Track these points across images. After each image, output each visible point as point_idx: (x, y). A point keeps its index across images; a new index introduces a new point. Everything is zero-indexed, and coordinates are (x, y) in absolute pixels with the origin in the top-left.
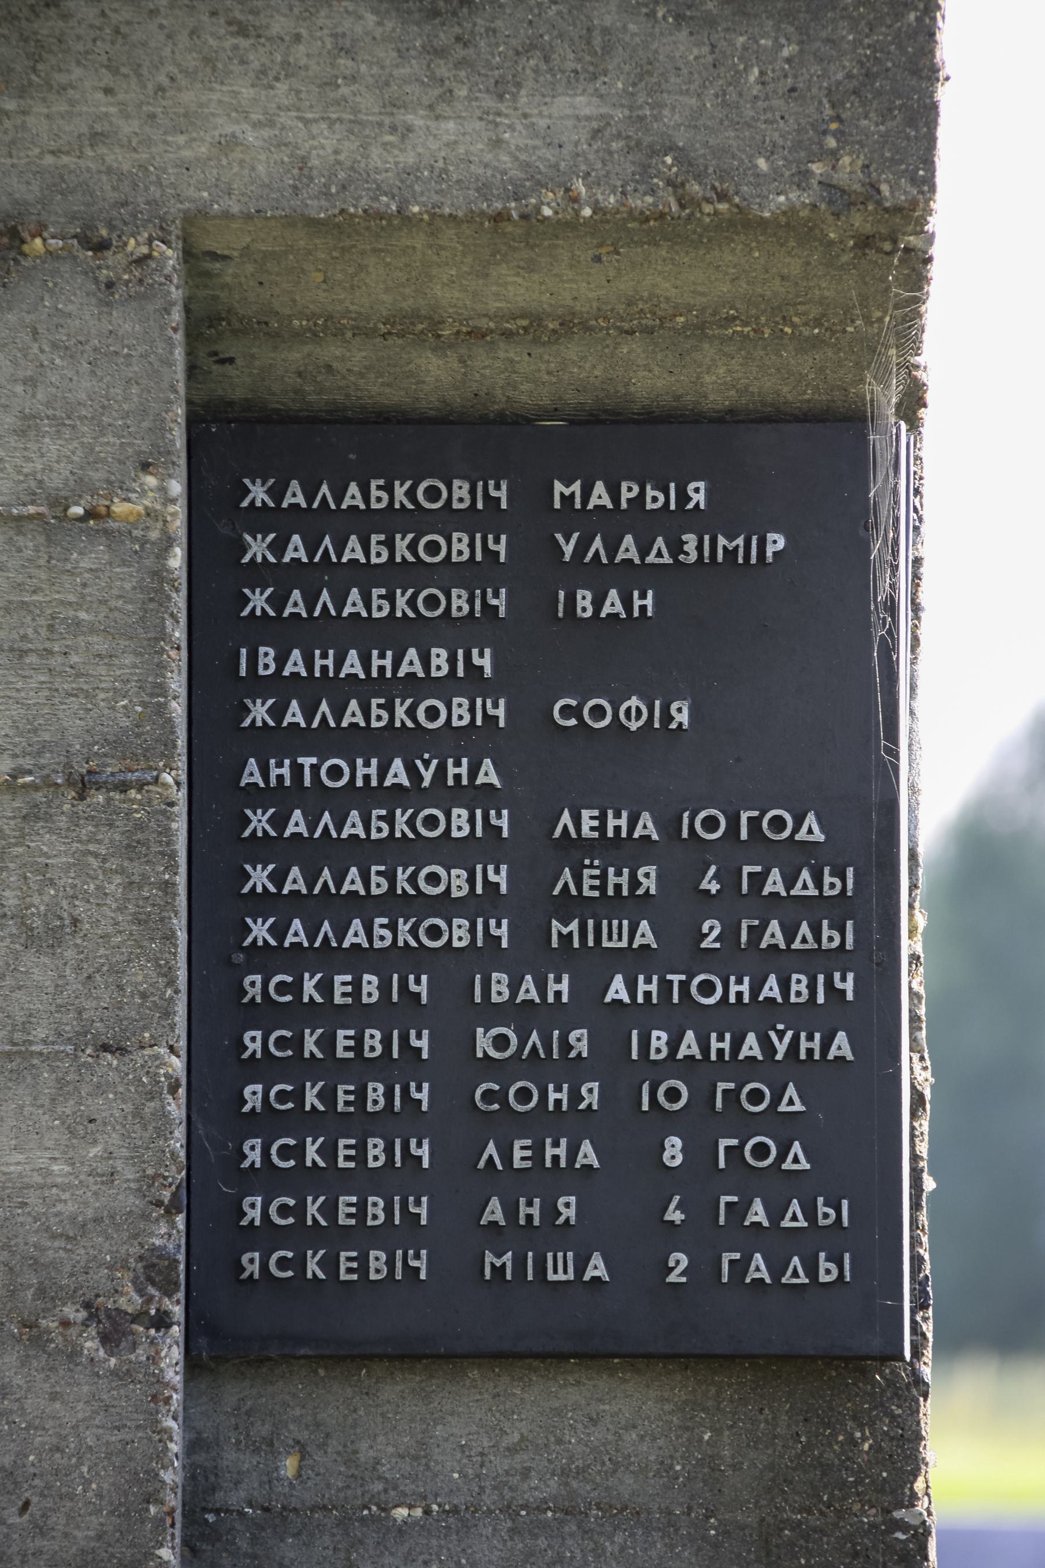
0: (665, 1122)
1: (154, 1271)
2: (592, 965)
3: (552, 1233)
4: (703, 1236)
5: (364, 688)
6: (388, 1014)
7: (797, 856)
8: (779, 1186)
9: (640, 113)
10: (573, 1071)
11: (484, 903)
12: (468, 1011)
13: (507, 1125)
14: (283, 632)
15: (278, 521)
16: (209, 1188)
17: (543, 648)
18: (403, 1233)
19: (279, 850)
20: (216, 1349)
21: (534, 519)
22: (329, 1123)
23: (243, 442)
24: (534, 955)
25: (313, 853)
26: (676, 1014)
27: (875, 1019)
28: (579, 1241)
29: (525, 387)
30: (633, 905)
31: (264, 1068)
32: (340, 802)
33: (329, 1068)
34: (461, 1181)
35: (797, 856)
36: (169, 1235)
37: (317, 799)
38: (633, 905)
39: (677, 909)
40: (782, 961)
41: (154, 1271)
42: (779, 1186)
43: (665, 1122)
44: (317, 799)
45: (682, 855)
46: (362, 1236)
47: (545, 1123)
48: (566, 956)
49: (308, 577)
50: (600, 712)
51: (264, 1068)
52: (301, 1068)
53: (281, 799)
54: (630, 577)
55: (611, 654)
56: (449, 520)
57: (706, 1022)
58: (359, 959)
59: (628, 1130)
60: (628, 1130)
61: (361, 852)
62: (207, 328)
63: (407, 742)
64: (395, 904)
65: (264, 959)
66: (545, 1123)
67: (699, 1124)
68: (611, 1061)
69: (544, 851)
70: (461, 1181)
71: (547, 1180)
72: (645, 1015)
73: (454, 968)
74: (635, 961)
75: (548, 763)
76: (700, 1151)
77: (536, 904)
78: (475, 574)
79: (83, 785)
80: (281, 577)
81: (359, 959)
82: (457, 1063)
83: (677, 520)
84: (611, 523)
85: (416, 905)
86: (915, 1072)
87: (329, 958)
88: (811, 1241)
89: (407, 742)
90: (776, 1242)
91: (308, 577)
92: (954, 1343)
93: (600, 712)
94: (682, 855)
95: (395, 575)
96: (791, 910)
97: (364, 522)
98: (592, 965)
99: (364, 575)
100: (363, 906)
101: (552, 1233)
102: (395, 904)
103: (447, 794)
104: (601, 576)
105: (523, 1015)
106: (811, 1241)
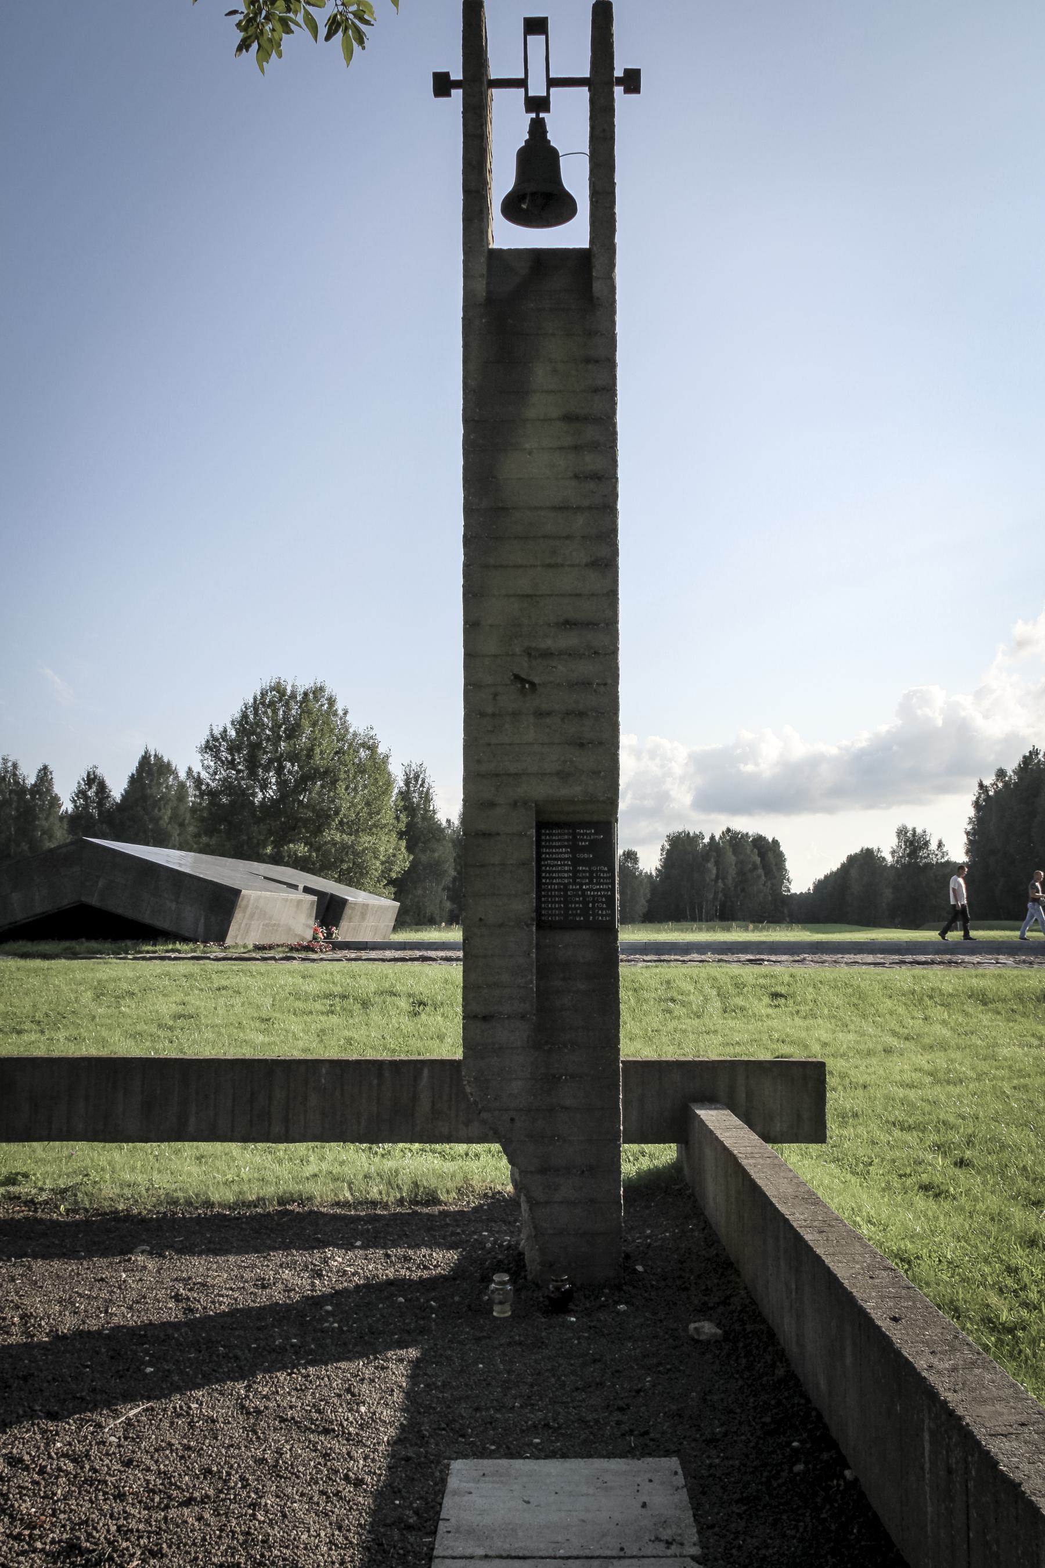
0: (589, 902)
1: (532, 919)
2: (581, 885)
3: (577, 915)
4: (594, 915)
5: (555, 853)
6: (559, 890)
7: (604, 872)
8: (602, 909)
9: (105, 1033)
10: (579, 896)
11: (569, 877)
12: (566, 890)
13: (572, 903)
14: (546, 847)
15: (546, 835)
16: (538, 910)
17: (575, 849)
18: (560, 915)
19: (546, 872)
20: (539, 927)
21: (574, 835)
22: (552, 902)
23: (542, 825)
24: (575, 883)
25: (550, 872)
26: (591, 890)
27: (613, 890)
28: (580, 915)
29: (106, 1204)
30: (586, 878)
31: (544, 896)
32: (553, 866)
33: (551, 896)
34: (567, 908)
35: (604, 872)
36: (534, 915)
37: (550, 866)
38: (586, 878)
39: (591, 878)
40: (603, 884)
41: (532, 919)
42: (602, 909)
43: (589, 902)
44: (550, 866)
45: (591, 872)
46: (555, 915)
47: (577, 902)
48: (579, 884)
49: (549, 841)
50: (582, 856)
51: (544, 896)
52: (548, 896)
53: (546, 866)
54: (585, 841)
55: (583, 849)
56: (565, 834)
57: (594, 890)
58: (555, 884)
59: (585, 903)
60: (585, 903)
61: (555, 872)
62: (538, 813)
63: (561, 859)
64: (559, 878)
65: (544, 884)
66: (577, 902)
67: (594, 902)
68: (583, 895)
69: (575, 872)
70: (567, 908)
71: (576, 909)
72: (587, 890)
73: (565, 885)
74: (586, 884)
75: (576, 862)
76: (593, 905)
77: (575, 877)
78: (568, 840)
79: (524, 864)
80: (546, 841)
81: (555, 884)
82: (566, 896)
83: (591, 834)
84: (583, 834)
85: (561, 878)
86: (617, 896)
87: (552, 884)
88: (606, 915)
89: (561, 859)
90: (602, 916)
91: (549, 841)
92: (623, 922)
93: (582, 856)
94: (591, 872)
95: (559, 840)
96: (604, 878)
97: (555, 834)
98: (581, 885)
99: (555, 841)
100: (555, 878)
101: (577, 915)
102: (559, 878)
103: (565, 865)
104: (582, 840)
105: (573, 890)
106: (606, 915)
